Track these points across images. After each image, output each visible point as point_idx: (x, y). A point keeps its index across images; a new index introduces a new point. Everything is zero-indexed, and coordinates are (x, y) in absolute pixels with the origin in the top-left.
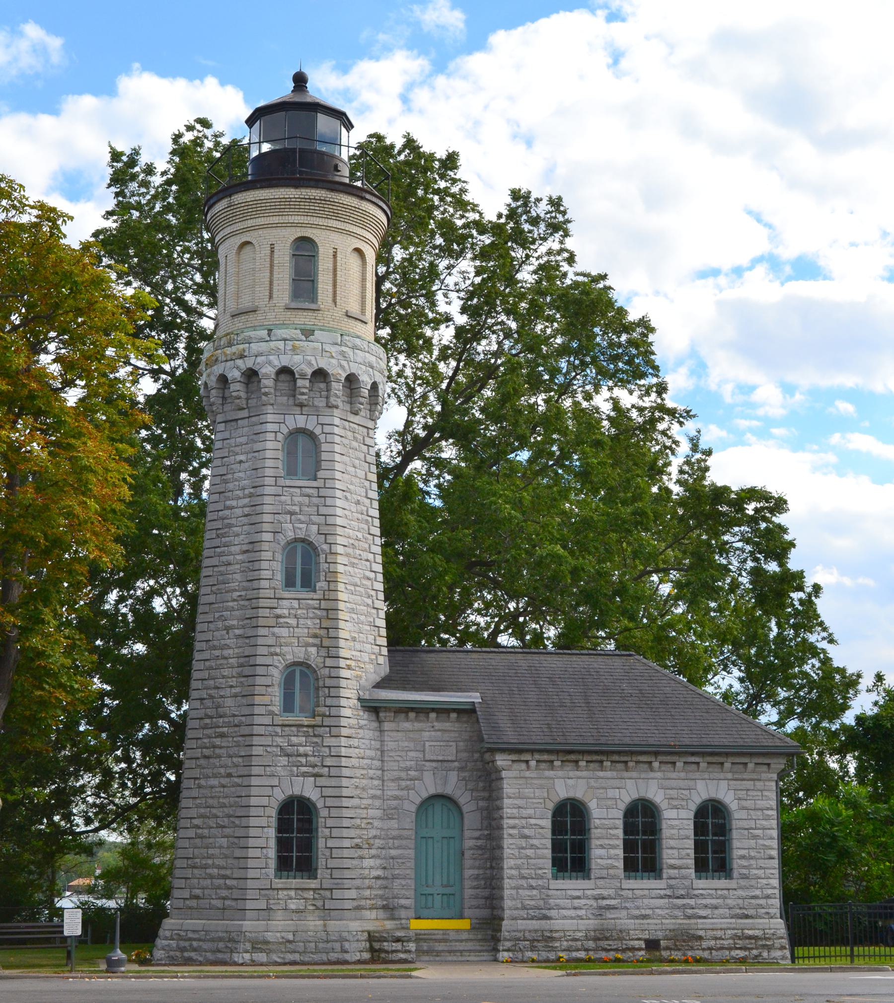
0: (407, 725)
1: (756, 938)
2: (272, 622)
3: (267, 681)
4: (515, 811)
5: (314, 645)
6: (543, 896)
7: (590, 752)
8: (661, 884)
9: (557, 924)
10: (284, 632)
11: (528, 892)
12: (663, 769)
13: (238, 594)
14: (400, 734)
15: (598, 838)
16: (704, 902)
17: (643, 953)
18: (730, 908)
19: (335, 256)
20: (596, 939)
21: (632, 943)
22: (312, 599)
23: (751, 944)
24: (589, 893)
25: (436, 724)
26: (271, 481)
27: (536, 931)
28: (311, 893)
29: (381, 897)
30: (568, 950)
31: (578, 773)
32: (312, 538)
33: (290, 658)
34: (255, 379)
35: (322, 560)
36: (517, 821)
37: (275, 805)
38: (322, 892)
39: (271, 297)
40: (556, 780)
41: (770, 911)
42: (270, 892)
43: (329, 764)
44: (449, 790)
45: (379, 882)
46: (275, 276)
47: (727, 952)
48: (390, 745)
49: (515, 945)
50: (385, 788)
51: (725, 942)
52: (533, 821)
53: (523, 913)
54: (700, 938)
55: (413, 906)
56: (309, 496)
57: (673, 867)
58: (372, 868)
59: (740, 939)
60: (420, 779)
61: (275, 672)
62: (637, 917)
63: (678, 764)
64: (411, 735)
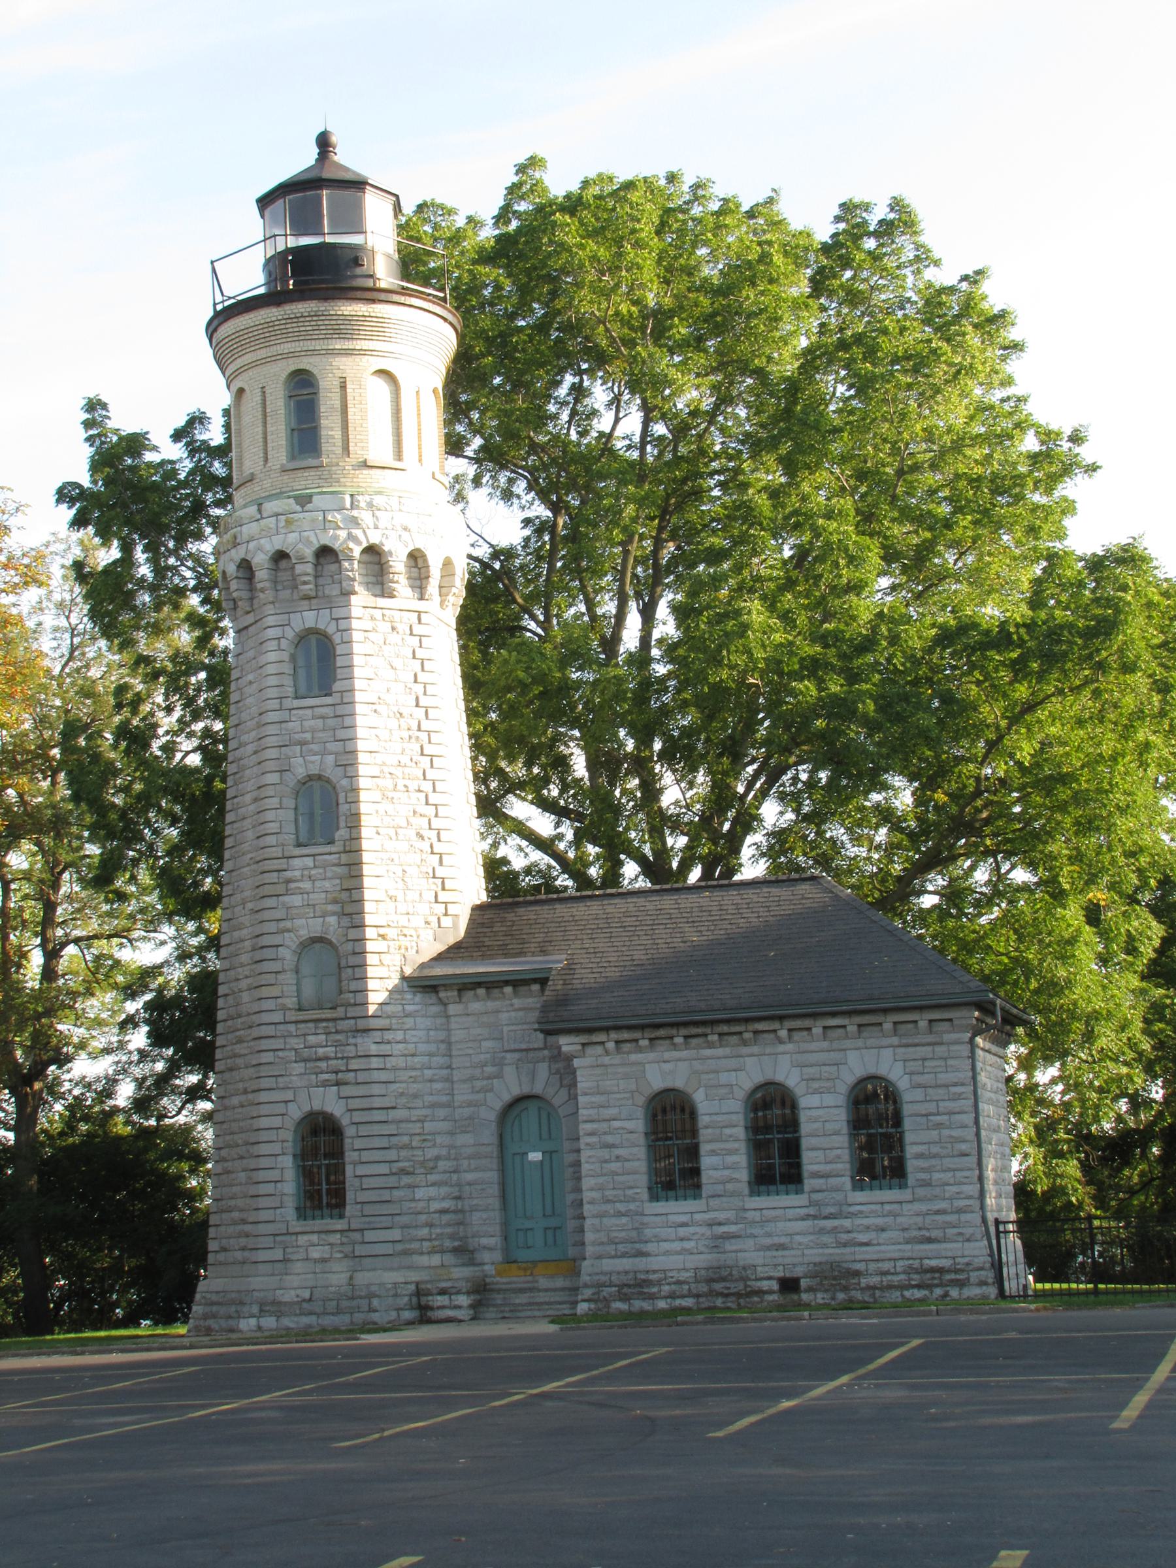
0: (476, 1006)
1: (941, 1270)
2: (281, 889)
4: (592, 1112)
5: (334, 914)
6: (637, 1225)
7: (685, 1024)
9: (655, 1263)
10: (296, 900)
11: (614, 1221)
12: (934, 1029)
13: (249, 856)
14: (470, 1018)
16: (865, 1222)
18: (904, 1230)
19: (343, 387)
20: (710, 1281)
21: (759, 1284)
22: (330, 854)
23: (934, 1278)
24: (697, 1217)
25: (515, 1001)
26: (274, 704)
27: (626, 1273)
28: (338, 1236)
29: (452, 1237)
30: (672, 1296)
33: (304, 934)
35: (341, 800)
37: (290, 1124)
38: (350, 1234)
39: (266, 460)
40: (647, 1066)
42: (288, 1238)
43: (355, 1067)
44: (538, 1089)
45: (446, 1218)
46: (260, 429)
47: (898, 1293)
48: (457, 1035)
49: (598, 1293)
50: (456, 1092)
51: (896, 1278)
52: (616, 1124)
53: (610, 1249)
54: (857, 1274)
55: (499, 1246)
56: (323, 717)
57: (816, 1175)
58: (430, 1199)
59: (917, 1272)
60: (499, 1076)
62: (769, 1248)
63: (814, 1030)
64: (485, 1019)
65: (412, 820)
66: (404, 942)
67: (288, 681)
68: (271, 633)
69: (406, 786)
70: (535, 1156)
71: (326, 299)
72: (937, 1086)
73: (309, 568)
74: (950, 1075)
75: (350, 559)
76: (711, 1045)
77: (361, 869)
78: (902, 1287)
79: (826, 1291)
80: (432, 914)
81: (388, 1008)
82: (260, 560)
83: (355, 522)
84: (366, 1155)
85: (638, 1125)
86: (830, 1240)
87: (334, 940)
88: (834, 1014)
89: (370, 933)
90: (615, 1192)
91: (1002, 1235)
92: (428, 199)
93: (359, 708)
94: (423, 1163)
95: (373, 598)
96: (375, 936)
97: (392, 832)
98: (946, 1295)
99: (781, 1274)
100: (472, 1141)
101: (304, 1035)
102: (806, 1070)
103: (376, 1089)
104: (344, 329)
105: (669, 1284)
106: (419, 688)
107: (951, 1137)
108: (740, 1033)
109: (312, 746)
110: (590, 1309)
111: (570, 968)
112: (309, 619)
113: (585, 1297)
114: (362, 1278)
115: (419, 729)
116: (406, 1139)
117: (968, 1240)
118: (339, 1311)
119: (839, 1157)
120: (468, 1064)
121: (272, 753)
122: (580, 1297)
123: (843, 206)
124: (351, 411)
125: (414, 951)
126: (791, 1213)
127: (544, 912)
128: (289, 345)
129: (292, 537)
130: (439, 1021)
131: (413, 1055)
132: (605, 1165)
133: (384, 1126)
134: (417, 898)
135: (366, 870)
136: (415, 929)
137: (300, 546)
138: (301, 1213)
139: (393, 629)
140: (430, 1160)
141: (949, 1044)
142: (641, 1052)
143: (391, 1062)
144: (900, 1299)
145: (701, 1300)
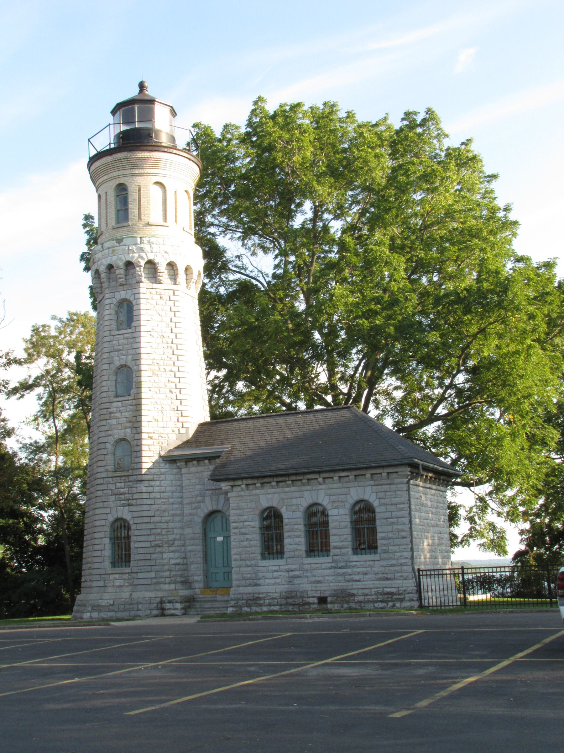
0: (193, 469)
1: (392, 594)
2: (107, 417)
4: (236, 518)
6: (255, 571)
7: (277, 476)
8: (329, 559)
9: (263, 589)
10: (114, 422)
14: (191, 475)
15: (288, 532)
16: (358, 570)
17: (316, 606)
18: (376, 574)
19: (139, 190)
20: (287, 598)
22: (128, 400)
23: (389, 598)
24: (282, 567)
27: (250, 594)
28: (127, 575)
29: (181, 576)
30: (270, 605)
31: (273, 490)
33: (117, 437)
35: (134, 376)
36: (237, 524)
37: (108, 524)
39: (107, 225)
41: (403, 574)
44: (220, 508)
47: (372, 605)
48: (185, 483)
49: (237, 603)
52: (247, 523)
53: (243, 582)
54: (353, 595)
55: (202, 581)
56: (127, 339)
57: (336, 548)
58: (170, 559)
59: (381, 595)
60: (203, 501)
61: (108, 446)
65: (167, 384)
66: (161, 440)
67: (114, 323)
68: (107, 301)
69: (165, 369)
70: (220, 539)
71: (131, 151)
72: (392, 504)
73: (122, 271)
74: (397, 499)
75: (140, 266)
76: (288, 486)
77: (141, 407)
78: (374, 602)
79: (339, 603)
80: (176, 427)
81: (152, 471)
82: (102, 269)
83: (142, 250)
84: (140, 538)
85: (256, 524)
86: (342, 579)
87: (129, 440)
88: (343, 470)
89: (144, 436)
90: (246, 556)
91: (421, 577)
92: (228, 123)
93: (142, 334)
94: (167, 542)
95: (151, 284)
96: (147, 438)
97: (157, 390)
98: (394, 606)
99: (319, 595)
100: (191, 532)
101: (116, 483)
103: (145, 508)
104: (139, 164)
105: (268, 599)
106: (173, 325)
107: (398, 529)
108: (301, 480)
109: (123, 352)
110: (233, 611)
111: (231, 451)
112: (123, 294)
113: (231, 605)
114: (136, 595)
115: (172, 343)
116: (159, 531)
117: (405, 579)
118: (124, 611)
119: (346, 539)
120: (189, 496)
121: (106, 356)
122: (229, 605)
123: (405, 113)
124: (142, 200)
125: (166, 445)
126: (324, 566)
127: (228, 426)
128: (115, 173)
130: (177, 476)
131: (164, 492)
132: (242, 543)
133: (148, 525)
134: (169, 420)
135: (143, 407)
136: (167, 434)
137: (118, 261)
138: (114, 564)
139: (161, 298)
140: (171, 540)
141: (397, 484)
142: (258, 490)
143: (152, 495)
144: (373, 608)
145: (283, 607)
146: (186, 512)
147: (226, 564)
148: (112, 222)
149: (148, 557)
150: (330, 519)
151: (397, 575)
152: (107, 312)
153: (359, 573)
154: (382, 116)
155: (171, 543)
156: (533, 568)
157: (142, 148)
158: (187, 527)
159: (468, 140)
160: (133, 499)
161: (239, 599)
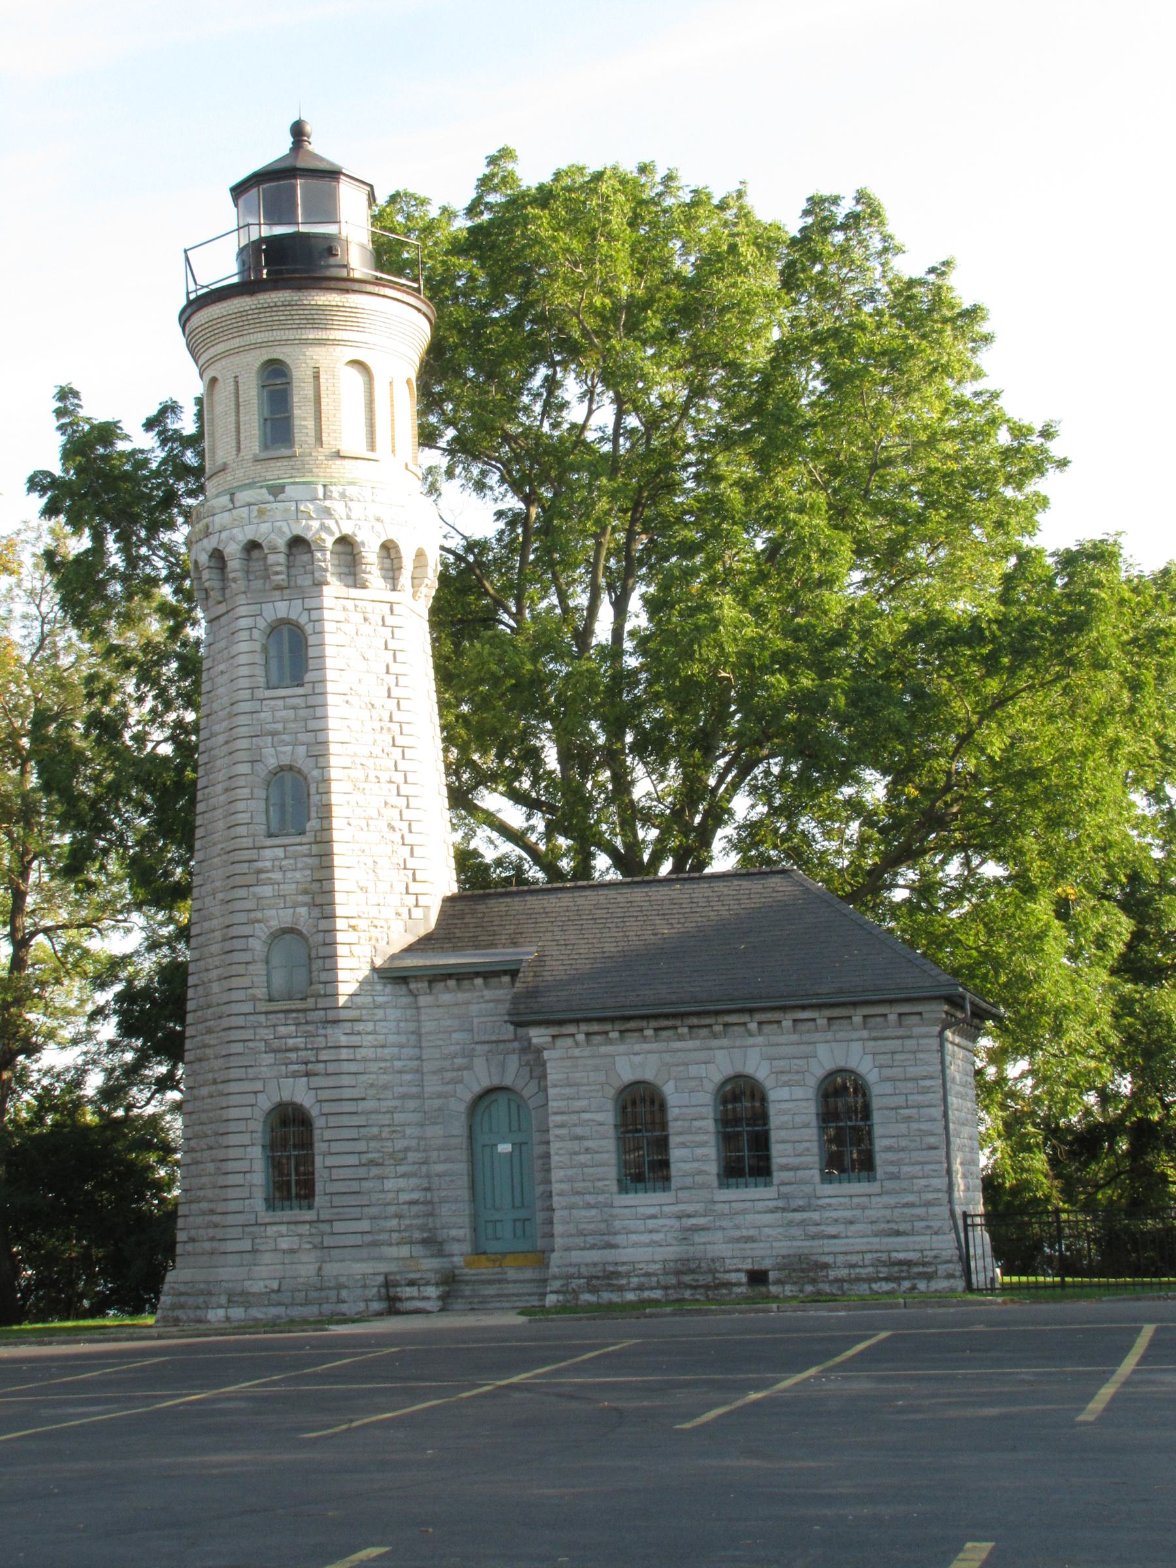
0: (446, 998)
1: (909, 1263)
2: (251, 879)
3: (247, 956)
4: (563, 1104)
7: (656, 1017)
8: (771, 1192)
10: (267, 891)
11: (584, 1213)
14: (440, 1010)
16: (834, 1214)
17: (743, 1289)
18: (872, 1223)
19: (317, 377)
20: (678, 1273)
24: (666, 1209)
25: (486, 993)
26: (246, 694)
27: (595, 1265)
28: (307, 1226)
29: (421, 1228)
30: (641, 1288)
31: (646, 1046)
32: (299, 764)
33: (275, 924)
34: (256, 554)
35: (313, 791)
37: (259, 1115)
39: (239, 450)
44: (508, 1081)
45: (415, 1209)
46: (233, 419)
47: (866, 1286)
48: (428, 1026)
53: (579, 1241)
54: (826, 1266)
56: (294, 708)
57: (785, 1168)
60: (469, 1067)
62: (738, 1240)
63: (784, 1023)
66: (375, 933)
68: (243, 623)
70: (505, 1148)
72: (906, 1079)
73: (282, 558)
75: (323, 549)
76: (681, 1038)
79: (795, 1283)
80: (403, 905)
81: (358, 1000)
83: (327, 512)
84: (336, 1146)
85: (608, 1117)
88: (803, 1008)
89: (340, 924)
94: (392, 1155)
97: (363, 823)
98: (914, 1288)
99: (750, 1267)
101: (274, 1026)
102: (775, 1063)
103: (346, 1080)
104: (318, 319)
106: (391, 680)
108: (710, 1026)
111: (540, 960)
112: (282, 609)
114: (331, 1269)
115: (391, 720)
116: (375, 1130)
118: (307, 1303)
119: (808, 1149)
121: (243, 744)
123: (810, 199)
124: (324, 401)
126: (760, 1205)
127: (516, 904)
129: (265, 527)
130: (409, 1012)
131: (383, 1046)
133: (355, 1117)
136: (386, 920)
137: (273, 536)
138: (270, 1204)
139: (365, 619)
141: (918, 1037)
145: (670, 1292)
146: (429, 1090)
147: (517, 1204)
148: (252, 444)
149: (355, 1186)
150: (773, 1110)
151: (919, 1225)
152: (244, 647)
153: (836, 1220)
154: (734, 187)
155: (398, 1158)
156: (1064, 1216)
157: (324, 284)
158: (433, 1124)
159: (943, 264)
160: (318, 1061)
161: (572, 1277)
